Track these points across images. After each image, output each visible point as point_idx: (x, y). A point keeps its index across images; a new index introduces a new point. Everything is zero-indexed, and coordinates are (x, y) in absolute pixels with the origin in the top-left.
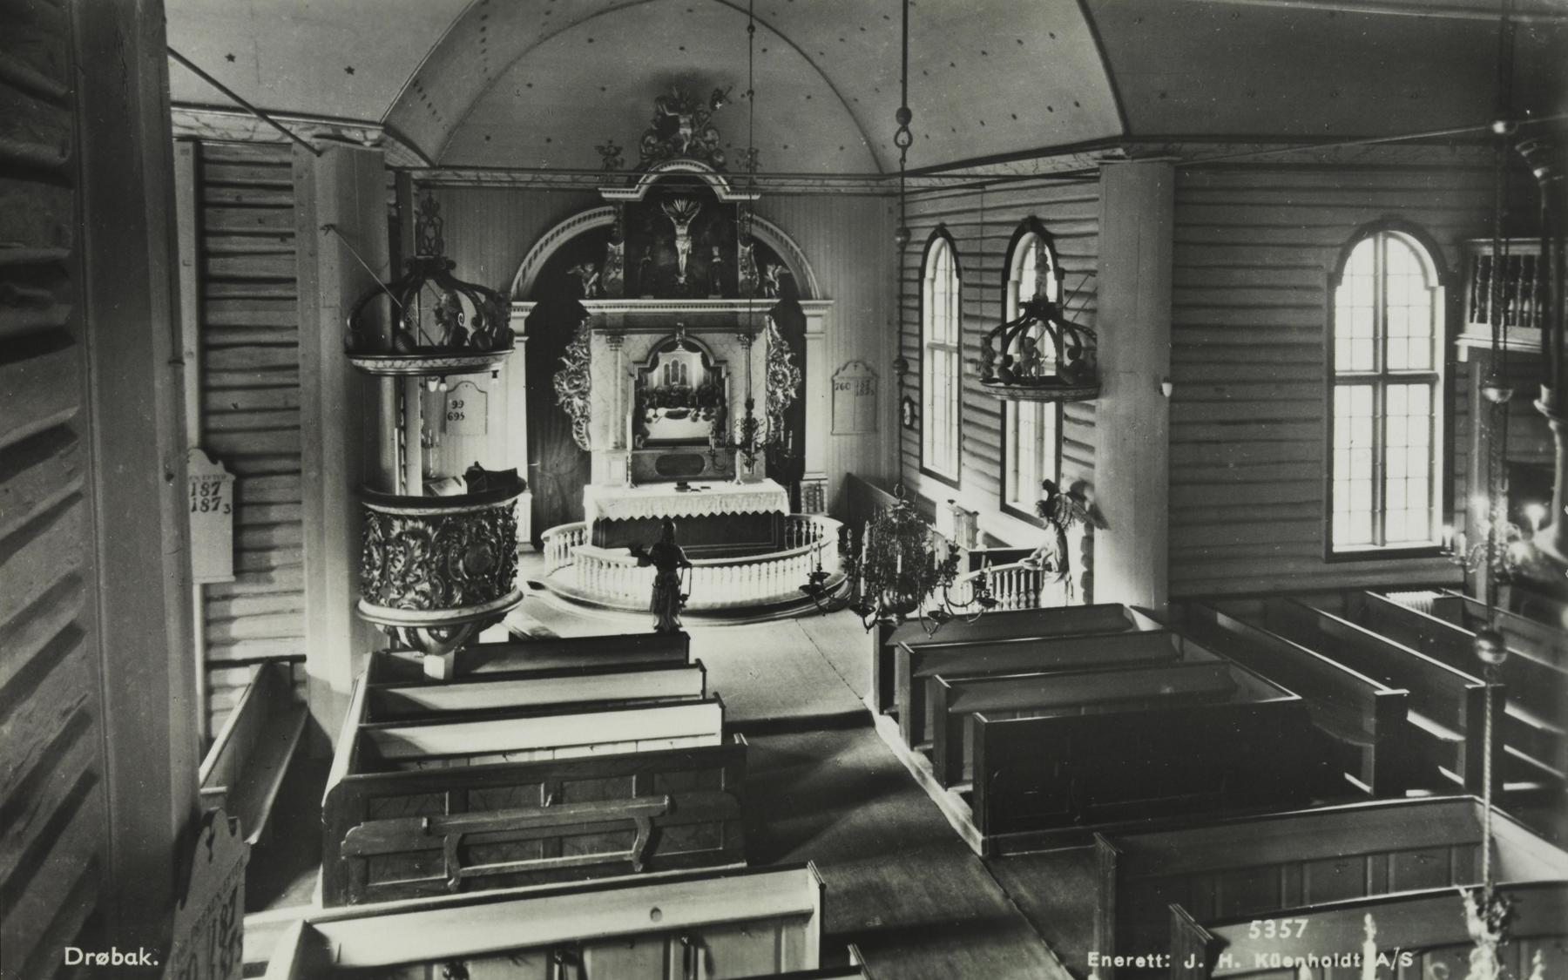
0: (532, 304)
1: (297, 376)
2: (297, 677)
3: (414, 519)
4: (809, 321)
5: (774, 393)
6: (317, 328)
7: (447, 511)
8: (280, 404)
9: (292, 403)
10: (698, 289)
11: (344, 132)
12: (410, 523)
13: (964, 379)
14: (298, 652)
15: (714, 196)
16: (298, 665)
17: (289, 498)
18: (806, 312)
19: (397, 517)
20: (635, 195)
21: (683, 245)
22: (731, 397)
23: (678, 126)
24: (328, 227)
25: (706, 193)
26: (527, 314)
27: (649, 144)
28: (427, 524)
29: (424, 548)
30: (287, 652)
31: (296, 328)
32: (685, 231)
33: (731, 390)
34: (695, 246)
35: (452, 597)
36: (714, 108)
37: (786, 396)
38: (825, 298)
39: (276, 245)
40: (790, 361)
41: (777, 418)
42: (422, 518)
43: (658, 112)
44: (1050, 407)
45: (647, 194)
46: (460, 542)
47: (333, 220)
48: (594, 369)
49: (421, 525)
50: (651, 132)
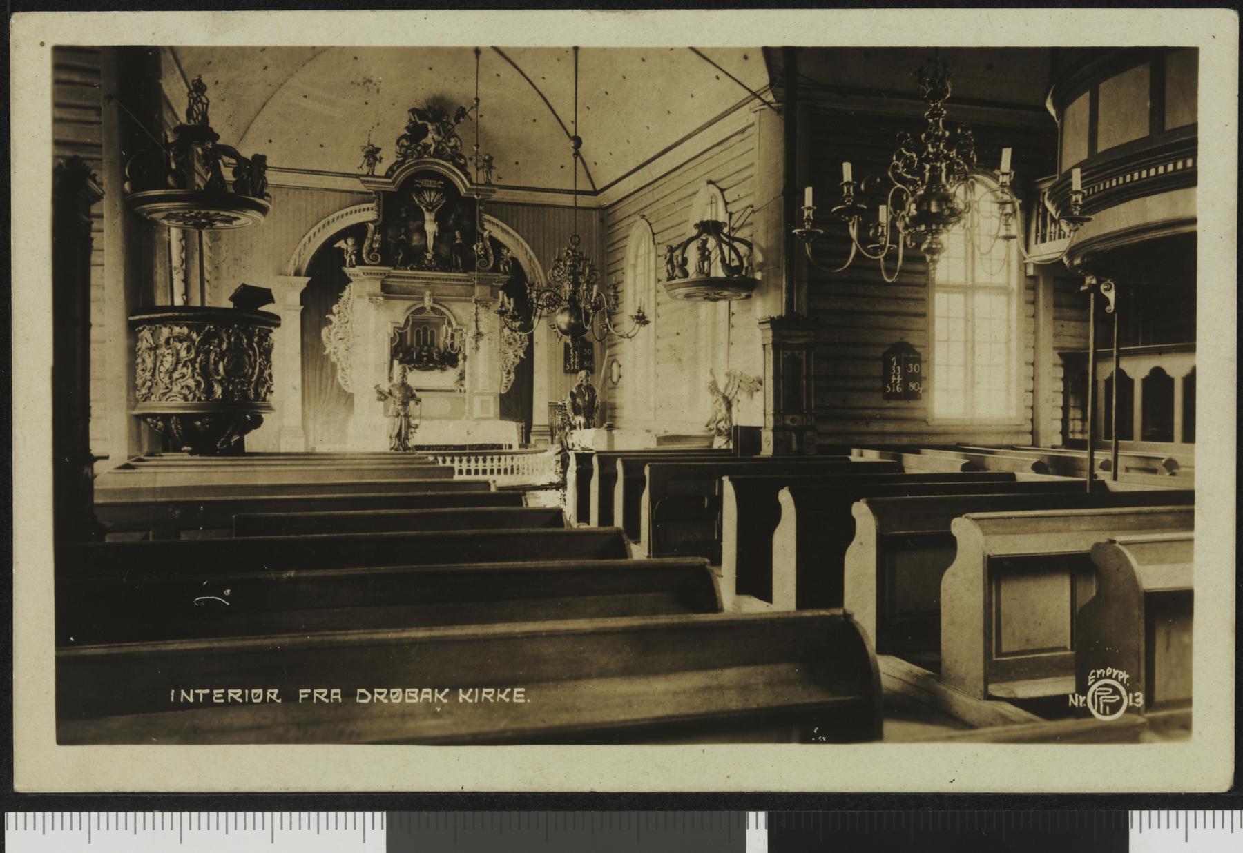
21: (431, 227)
25: (449, 188)
27: (403, 146)
29: (188, 350)
32: (433, 217)
41: (509, 373)
50: (404, 136)
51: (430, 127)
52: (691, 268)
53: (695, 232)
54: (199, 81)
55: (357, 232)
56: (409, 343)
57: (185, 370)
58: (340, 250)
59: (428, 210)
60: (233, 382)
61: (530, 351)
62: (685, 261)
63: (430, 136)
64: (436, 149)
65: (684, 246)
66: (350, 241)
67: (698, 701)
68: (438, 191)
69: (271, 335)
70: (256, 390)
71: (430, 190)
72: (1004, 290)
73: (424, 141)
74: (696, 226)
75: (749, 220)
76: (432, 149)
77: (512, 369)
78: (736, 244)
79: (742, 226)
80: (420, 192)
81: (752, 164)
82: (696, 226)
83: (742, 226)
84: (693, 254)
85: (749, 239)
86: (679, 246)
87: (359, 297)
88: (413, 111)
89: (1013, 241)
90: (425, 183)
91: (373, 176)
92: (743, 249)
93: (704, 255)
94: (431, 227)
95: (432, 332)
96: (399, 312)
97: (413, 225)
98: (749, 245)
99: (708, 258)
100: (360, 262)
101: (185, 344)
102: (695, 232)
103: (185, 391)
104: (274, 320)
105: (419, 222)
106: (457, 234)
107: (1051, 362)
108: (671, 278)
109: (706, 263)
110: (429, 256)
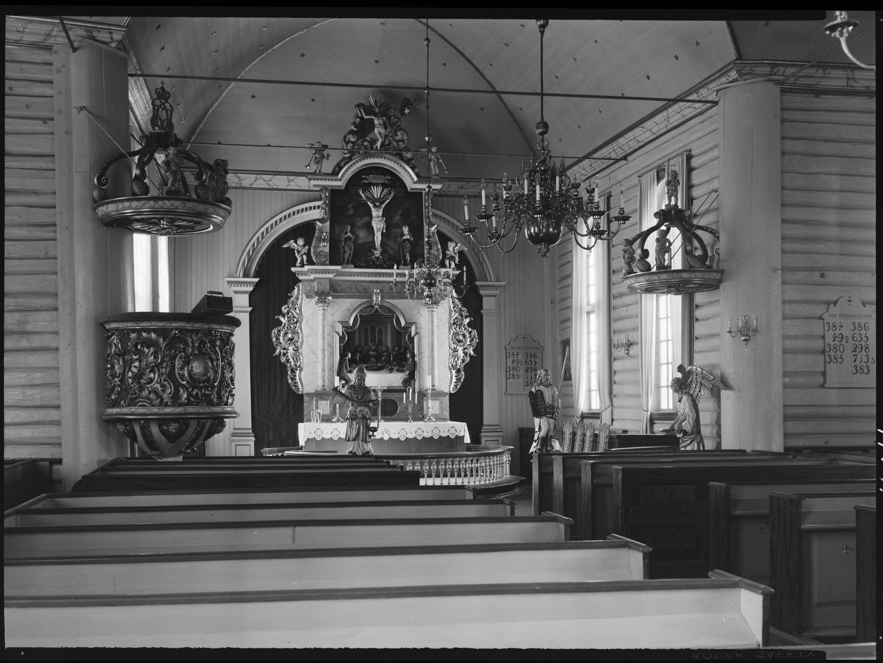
0: (257, 280)
1: (55, 232)
2: (55, 476)
3: (148, 331)
4: (485, 299)
5: (455, 350)
6: (73, 277)
7: (174, 325)
8: (41, 254)
9: (52, 253)
10: (390, 260)
11: (95, 34)
12: (144, 335)
13: (613, 350)
14: (57, 456)
15: (403, 185)
16: (55, 467)
17: (50, 329)
18: (482, 292)
19: (133, 331)
20: (339, 183)
21: (378, 225)
22: (420, 353)
23: (373, 126)
24: (82, 108)
25: (395, 182)
26: (251, 289)
27: (349, 142)
28: (159, 335)
29: (155, 354)
30: (48, 456)
31: (55, 225)
32: (380, 213)
33: (419, 346)
34: (389, 226)
35: (180, 397)
36: (403, 114)
37: (466, 354)
38: (498, 280)
39: (39, 126)
40: (469, 324)
41: (458, 371)
42: (155, 331)
43: (357, 116)
44: (709, 445)
45: (350, 183)
46: (184, 350)
47: (85, 103)
48: (305, 328)
49: (153, 335)
50: (351, 132)
51: (376, 122)
52: (652, 260)
53: (655, 222)
54: (163, 88)
55: (306, 231)
56: (357, 343)
57: (152, 375)
58: (291, 251)
59: (375, 206)
60: (197, 387)
61: (479, 349)
62: (646, 253)
63: (376, 131)
64: (382, 144)
65: (645, 235)
66: (301, 242)
68: (384, 186)
69: (233, 339)
70: (219, 393)
71: (377, 185)
72: (590, 409)
73: (371, 136)
74: (656, 215)
75: (715, 204)
76: (379, 144)
77: (462, 369)
78: (699, 232)
79: (707, 212)
80: (367, 187)
81: (716, 146)
82: (656, 215)
83: (707, 212)
84: (651, 244)
85: (713, 227)
86: (639, 236)
87: (308, 297)
88: (359, 106)
89: (291, 542)
90: (372, 178)
91: (320, 173)
92: (706, 237)
93: (664, 247)
94: (378, 225)
95: (380, 330)
96: (344, 310)
97: (360, 222)
98: (713, 232)
99: (668, 250)
100: (310, 262)
101: (152, 350)
102: (655, 222)
103: (153, 396)
104: (236, 323)
105: (366, 219)
106: (406, 230)
107: (65, 461)
108: (631, 271)
109: (667, 256)
110: (377, 253)
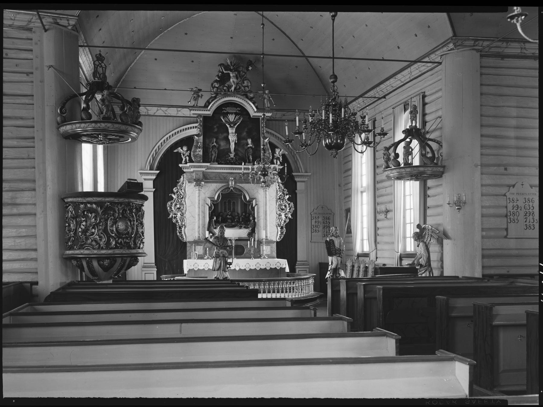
0: (158, 172)
1: (34, 142)
2: (34, 292)
3: (91, 203)
4: (298, 184)
5: (280, 215)
6: (45, 170)
7: (107, 199)
8: (25, 156)
9: (32, 155)
10: (240, 159)
11: (58, 21)
12: (89, 205)
13: (377, 215)
14: (35, 280)
15: (248, 113)
16: (34, 287)
17: (30, 202)
18: (296, 179)
19: (82, 203)
20: (209, 112)
21: (232, 138)
22: (258, 217)
23: (229, 77)
24: (50, 67)
25: (243, 112)
26: (154, 177)
27: (215, 87)
28: (97, 206)
29: (96, 217)
30: (29, 280)
31: (34, 138)
32: (234, 131)
33: (258, 213)
34: (239, 138)
35: (111, 244)
36: (248, 70)
37: (286, 217)
38: (306, 172)
39: (24, 78)
40: (288, 199)
41: (282, 228)
42: (95, 203)
43: (220, 71)
44: (436, 273)
45: (215, 112)
46: (113, 215)
47: (52, 63)
48: (188, 201)
49: (94, 206)
50: (216, 81)
51: (231, 75)
52: (401, 160)
53: (403, 136)
55: (188, 142)
56: (219, 211)
57: (93, 230)
58: (179, 154)
59: (231, 127)
60: (121, 238)
61: (295, 214)
62: (397, 156)
63: (231, 80)
64: (235, 89)
65: (396, 144)
66: (185, 148)
67: (370, 193)
68: (236, 114)
69: (143, 208)
70: (134, 241)
71: (232, 113)
73: (228, 83)
74: (403, 132)
75: (440, 125)
76: (233, 88)
78: (430, 143)
79: (435, 130)
80: (226, 115)
81: (441, 90)
82: (403, 132)
83: (435, 130)
84: (400, 150)
85: (439, 139)
86: (393, 145)
87: (189, 182)
88: (221, 65)
89: (179, 333)
90: (228, 110)
91: (197, 107)
92: (434, 145)
93: (408, 151)
94: (232, 138)
95: (234, 203)
96: (212, 190)
97: (221, 136)
98: (438, 143)
99: (411, 153)
100: (191, 161)
101: (93, 215)
102: (403, 136)
103: (94, 243)
104: (145, 198)
105: (225, 134)
106: (249, 141)
107: (40, 283)
108: (388, 167)
109: (410, 157)
110: (232, 156)
